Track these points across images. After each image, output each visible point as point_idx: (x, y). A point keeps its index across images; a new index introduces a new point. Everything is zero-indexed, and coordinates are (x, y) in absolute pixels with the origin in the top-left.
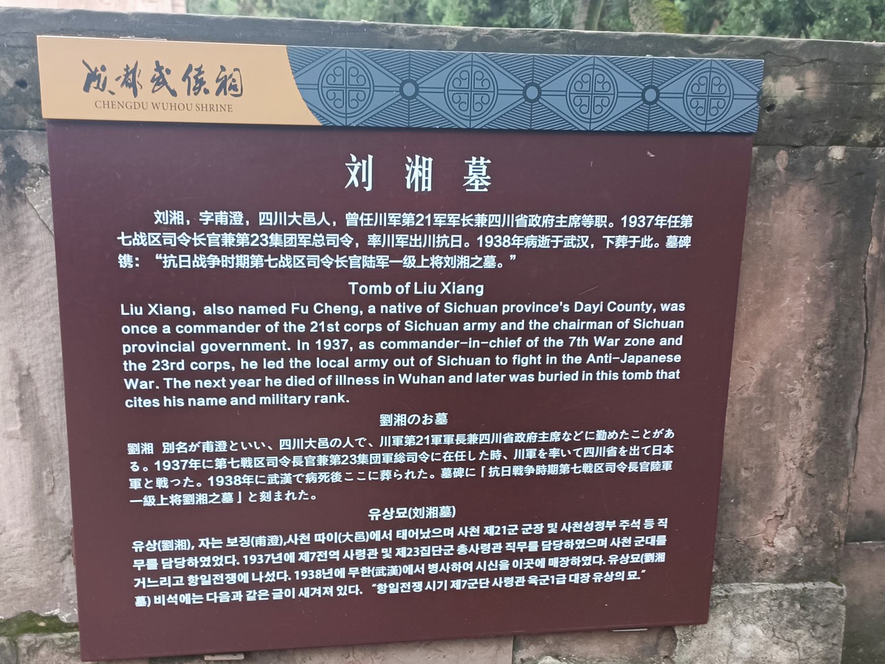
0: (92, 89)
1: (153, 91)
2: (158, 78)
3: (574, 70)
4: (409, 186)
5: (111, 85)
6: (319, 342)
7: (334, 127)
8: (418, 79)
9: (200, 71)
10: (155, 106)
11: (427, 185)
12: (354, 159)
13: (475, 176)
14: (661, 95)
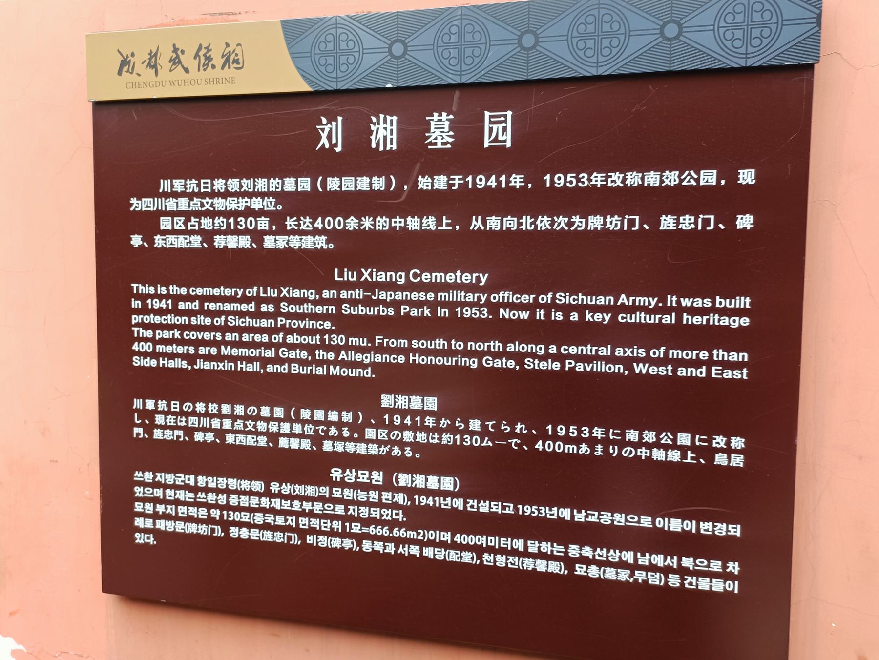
0: (124, 73)
1: (171, 71)
2: (175, 59)
3: (575, 13)
4: (373, 146)
5: (140, 68)
6: (459, 309)
7: (326, 92)
8: (682, 19)
9: (208, 49)
10: (172, 83)
11: (391, 144)
12: (324, 121)
13: (438, 132)
14: (409, 49)
